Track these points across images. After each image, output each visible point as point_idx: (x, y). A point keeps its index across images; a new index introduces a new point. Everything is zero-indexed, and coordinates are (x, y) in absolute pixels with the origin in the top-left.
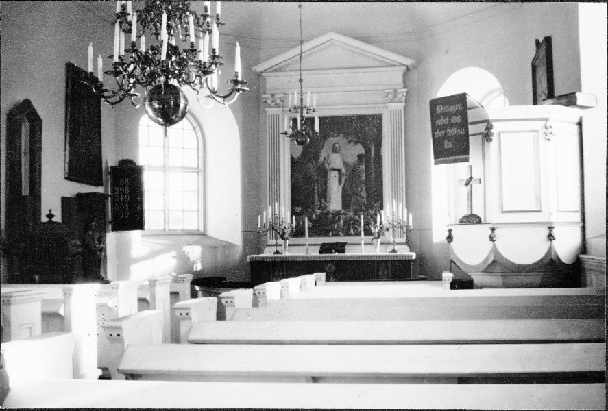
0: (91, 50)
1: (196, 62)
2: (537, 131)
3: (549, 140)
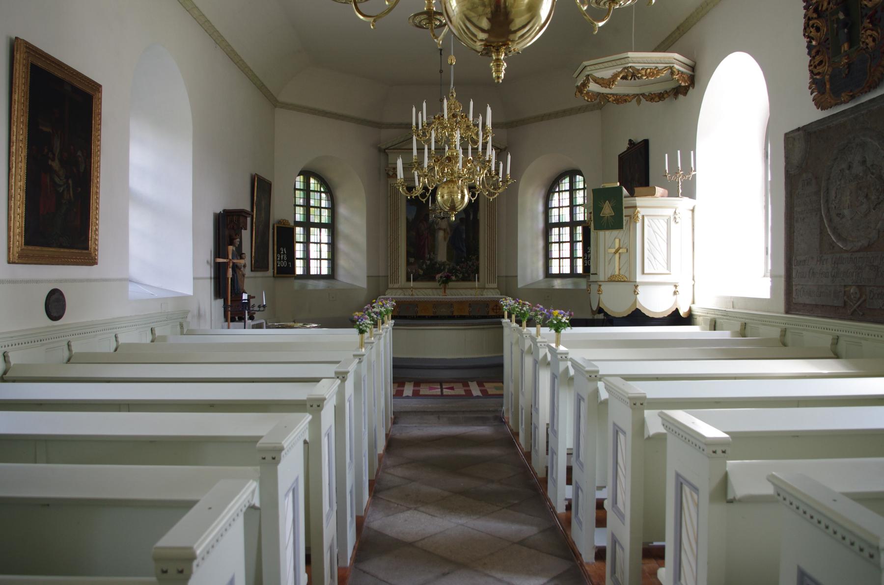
0: (414, 109)
1: (544, 492)
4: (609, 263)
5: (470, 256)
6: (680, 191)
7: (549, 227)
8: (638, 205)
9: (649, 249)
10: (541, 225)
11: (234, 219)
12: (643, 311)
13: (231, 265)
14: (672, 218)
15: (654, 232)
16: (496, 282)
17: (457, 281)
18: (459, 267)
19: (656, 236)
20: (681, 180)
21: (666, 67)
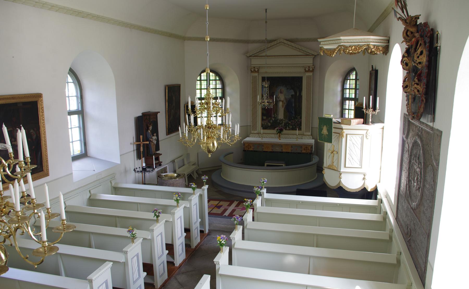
2: (363, 135)
3: (368, 139)
4: (329, 158)
5: (297, 116)
6: (370, 120)
7: (344, 99)
8: (343, 128)
9: (350, 153)
10: (339, 98)
11: (148, 118)
12: (344, 188)
13: (142, 145)
14: (365, 136)
15: (353, 144)
16: (310, 132)
17: (289, 130)
18: (290, 122)
19: (354, 146)
20: (371, 114)
21: (365, 45)
